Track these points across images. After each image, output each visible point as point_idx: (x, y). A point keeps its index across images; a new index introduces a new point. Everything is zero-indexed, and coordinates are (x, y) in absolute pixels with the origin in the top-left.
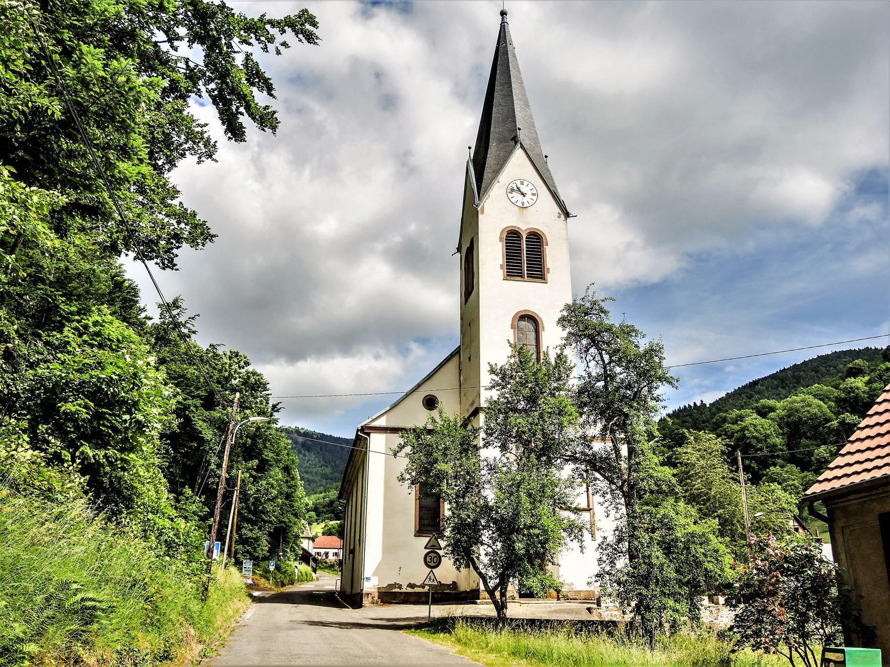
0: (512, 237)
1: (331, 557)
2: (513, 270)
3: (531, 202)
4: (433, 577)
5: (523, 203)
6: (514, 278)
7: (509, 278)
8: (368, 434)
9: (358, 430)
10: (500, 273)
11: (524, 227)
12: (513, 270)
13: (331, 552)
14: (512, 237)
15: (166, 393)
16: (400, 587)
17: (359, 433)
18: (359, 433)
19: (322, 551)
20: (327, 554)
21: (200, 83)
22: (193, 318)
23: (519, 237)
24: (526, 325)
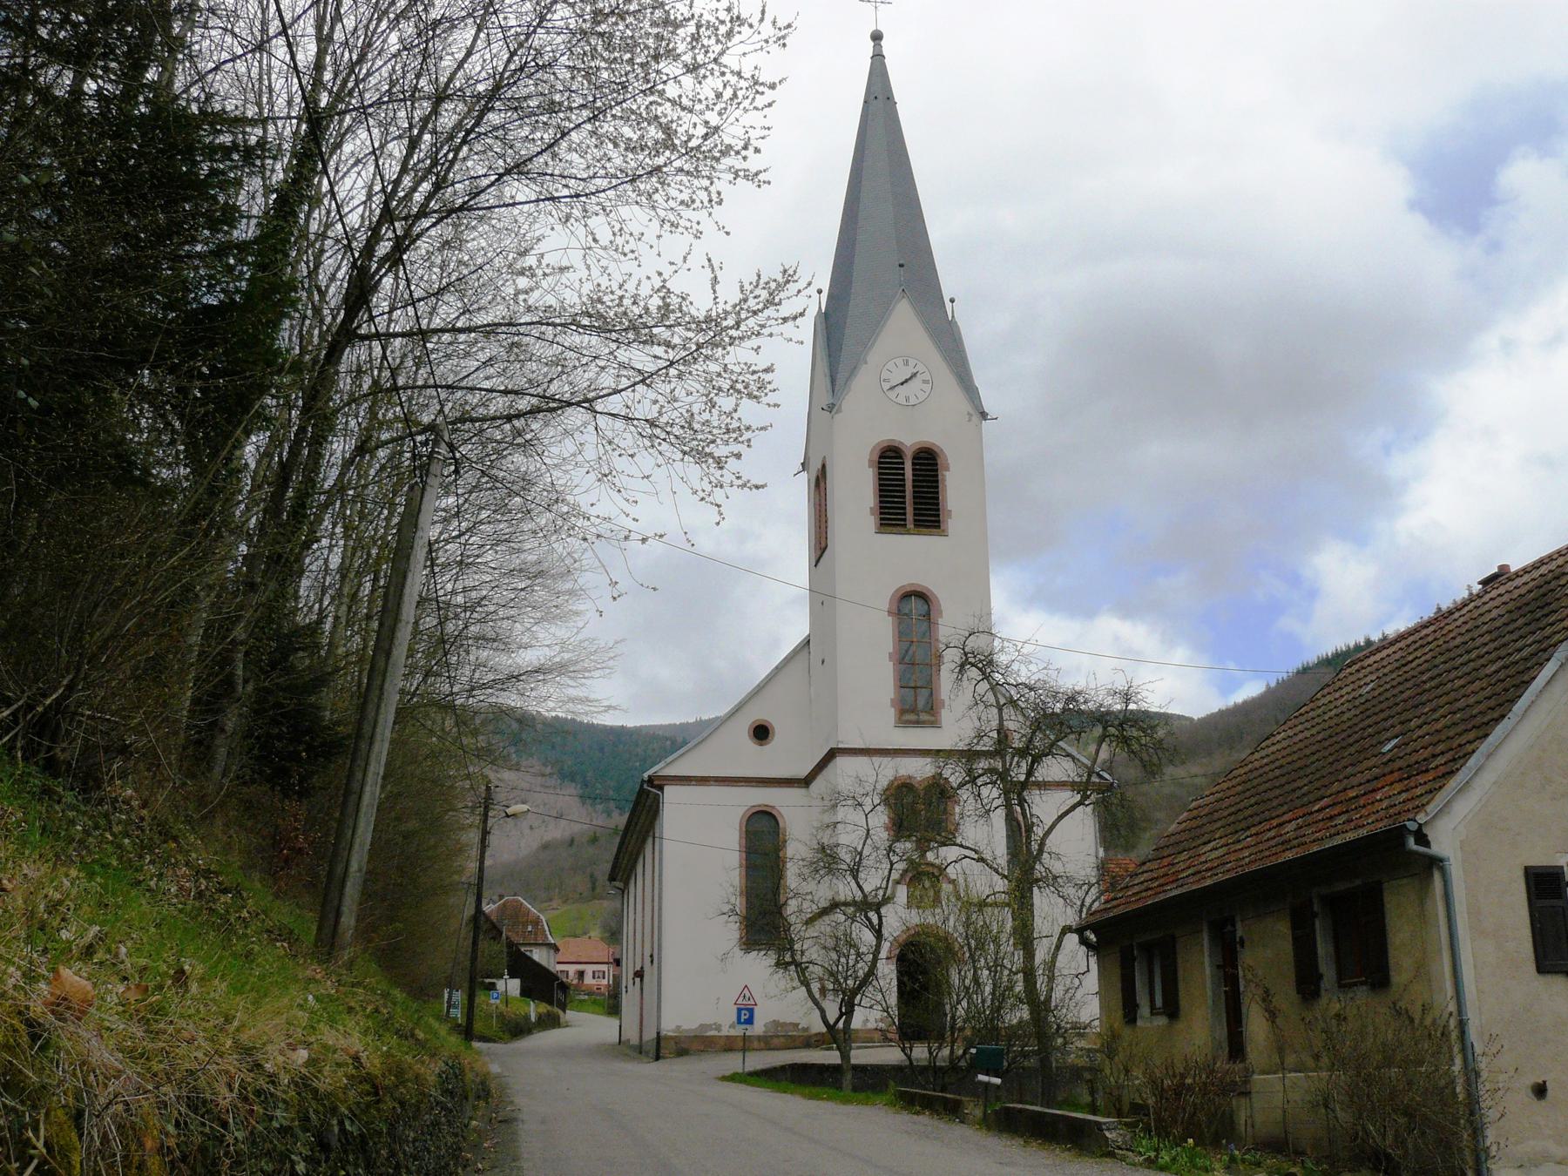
0: (888, 458)
1: (588, 980)
2: (890, 515)
3: (922, 396)
4: (748, 995)
5: (907, 399)
6: (895, 529)
7: (883, 529)
8: (661, 788)
9: (643, 781)
10: (871, 522)
11: (909, 440)
12: (890, 515)
13: (589, 969)
14: (888, 458)
15: (474, 1122)
16: (718, 1028)
17: (645, 786)
18: (645, 786)
19: (572, 969)
20: (581, 974)
21: (245, 231)
22: (716, 298)
23: (901, 457)
24: (915, 605)
